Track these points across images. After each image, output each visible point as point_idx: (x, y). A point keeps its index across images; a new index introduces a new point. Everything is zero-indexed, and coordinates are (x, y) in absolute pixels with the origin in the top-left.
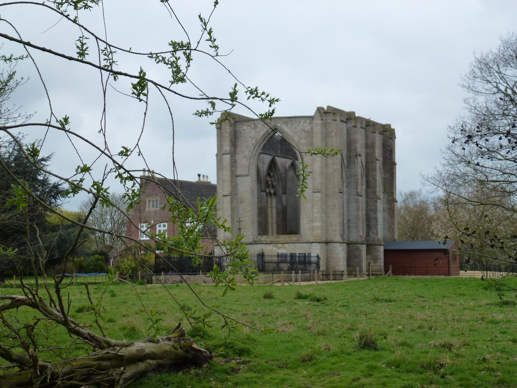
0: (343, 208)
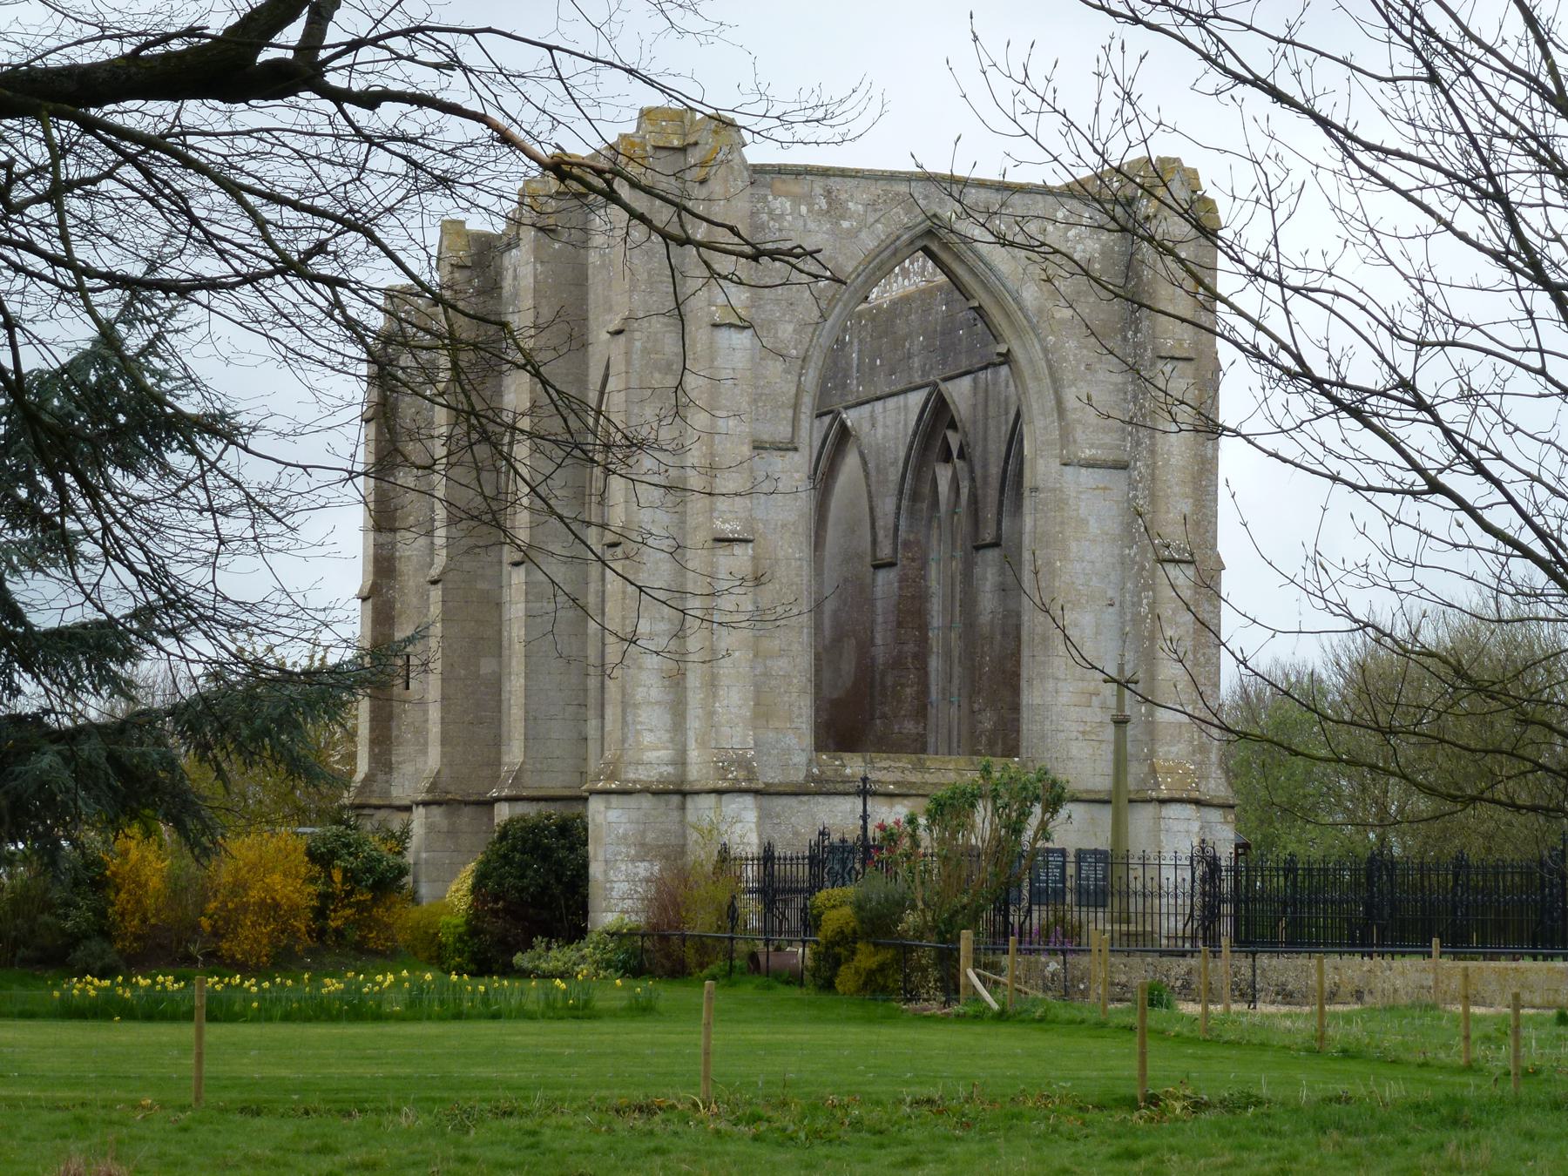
0: (953, 584)
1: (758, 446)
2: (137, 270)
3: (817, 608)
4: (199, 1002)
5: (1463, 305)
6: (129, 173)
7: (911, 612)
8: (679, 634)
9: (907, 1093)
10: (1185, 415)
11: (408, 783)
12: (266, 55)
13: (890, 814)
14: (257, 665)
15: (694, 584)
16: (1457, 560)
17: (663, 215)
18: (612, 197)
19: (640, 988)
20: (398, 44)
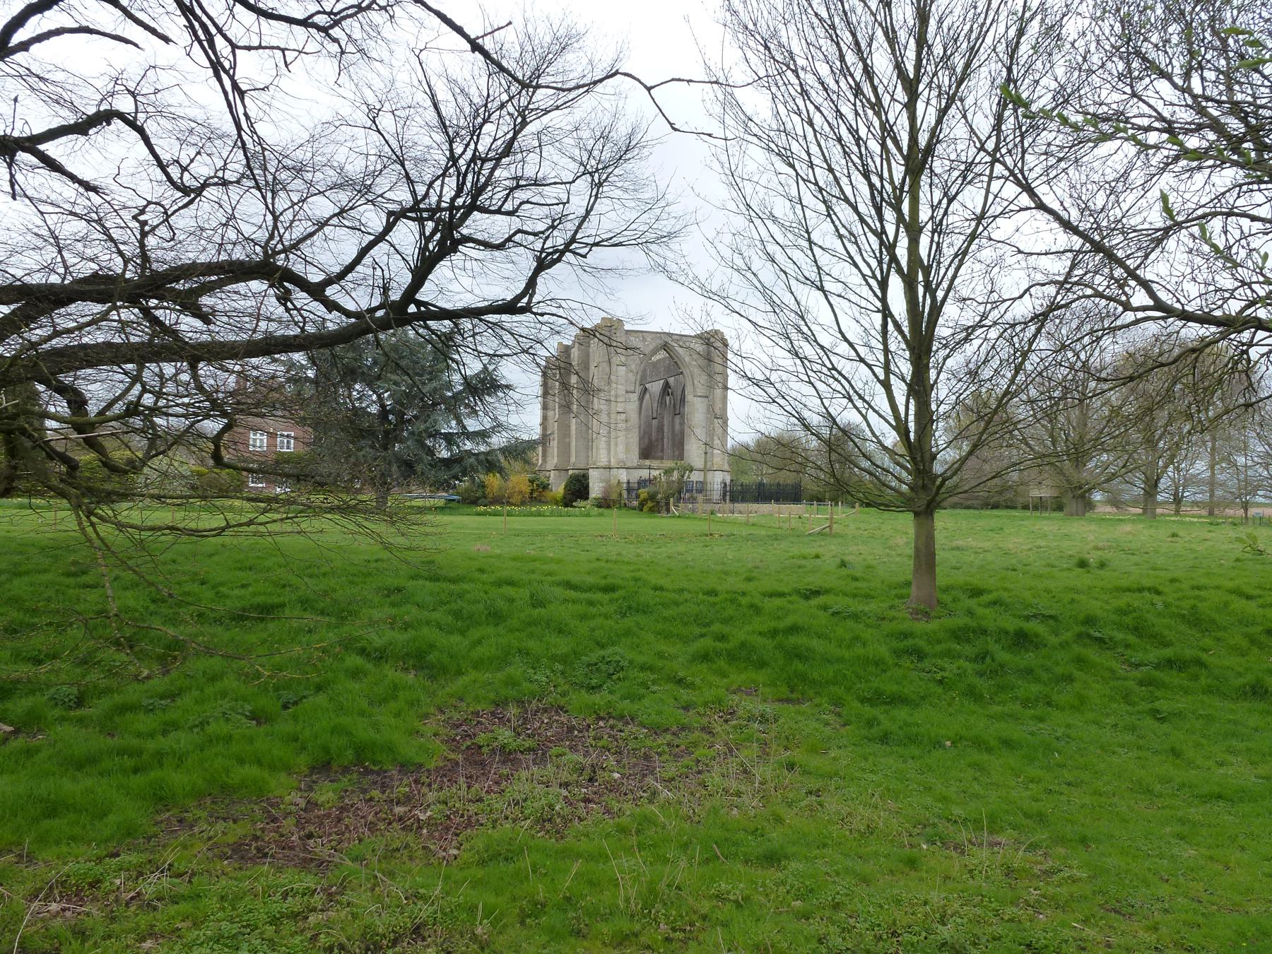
1: (627, 392)
2: (492, 352)
3: (640, 427)
4: (505, 512)
5: (781, 362)
6: (490, 331)
7: (660, 429)
8: (609, 433)
9: (659, 533)
10: (720, 385)
11: (550, 466)
12: (519, 305)
13: (655, 473)
14: (517, 439)
15: (613, 421)
16: (778, 417)
17: (606, 340)
18: (595, 336)
19: (601, 510)
20: (548, 302)
